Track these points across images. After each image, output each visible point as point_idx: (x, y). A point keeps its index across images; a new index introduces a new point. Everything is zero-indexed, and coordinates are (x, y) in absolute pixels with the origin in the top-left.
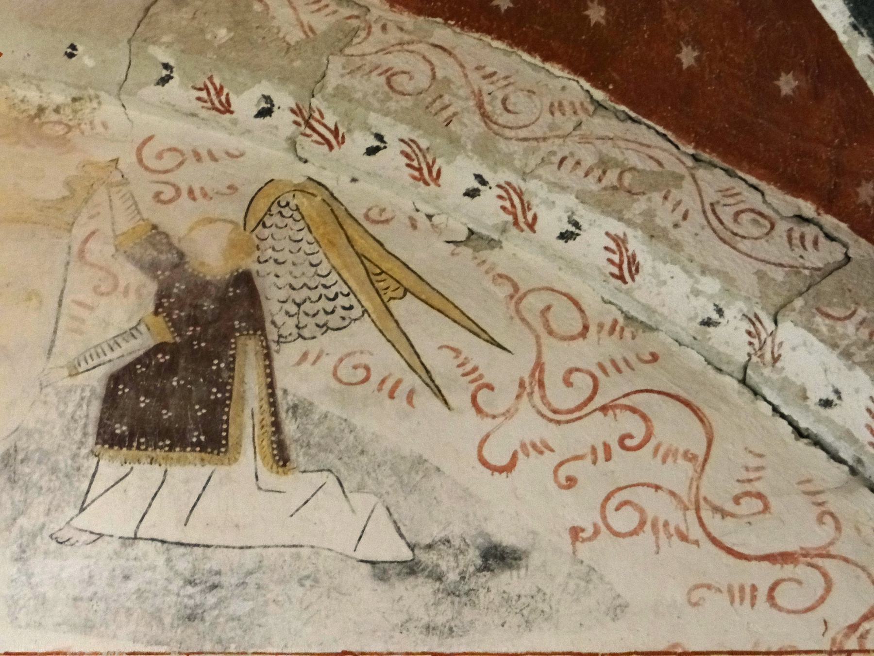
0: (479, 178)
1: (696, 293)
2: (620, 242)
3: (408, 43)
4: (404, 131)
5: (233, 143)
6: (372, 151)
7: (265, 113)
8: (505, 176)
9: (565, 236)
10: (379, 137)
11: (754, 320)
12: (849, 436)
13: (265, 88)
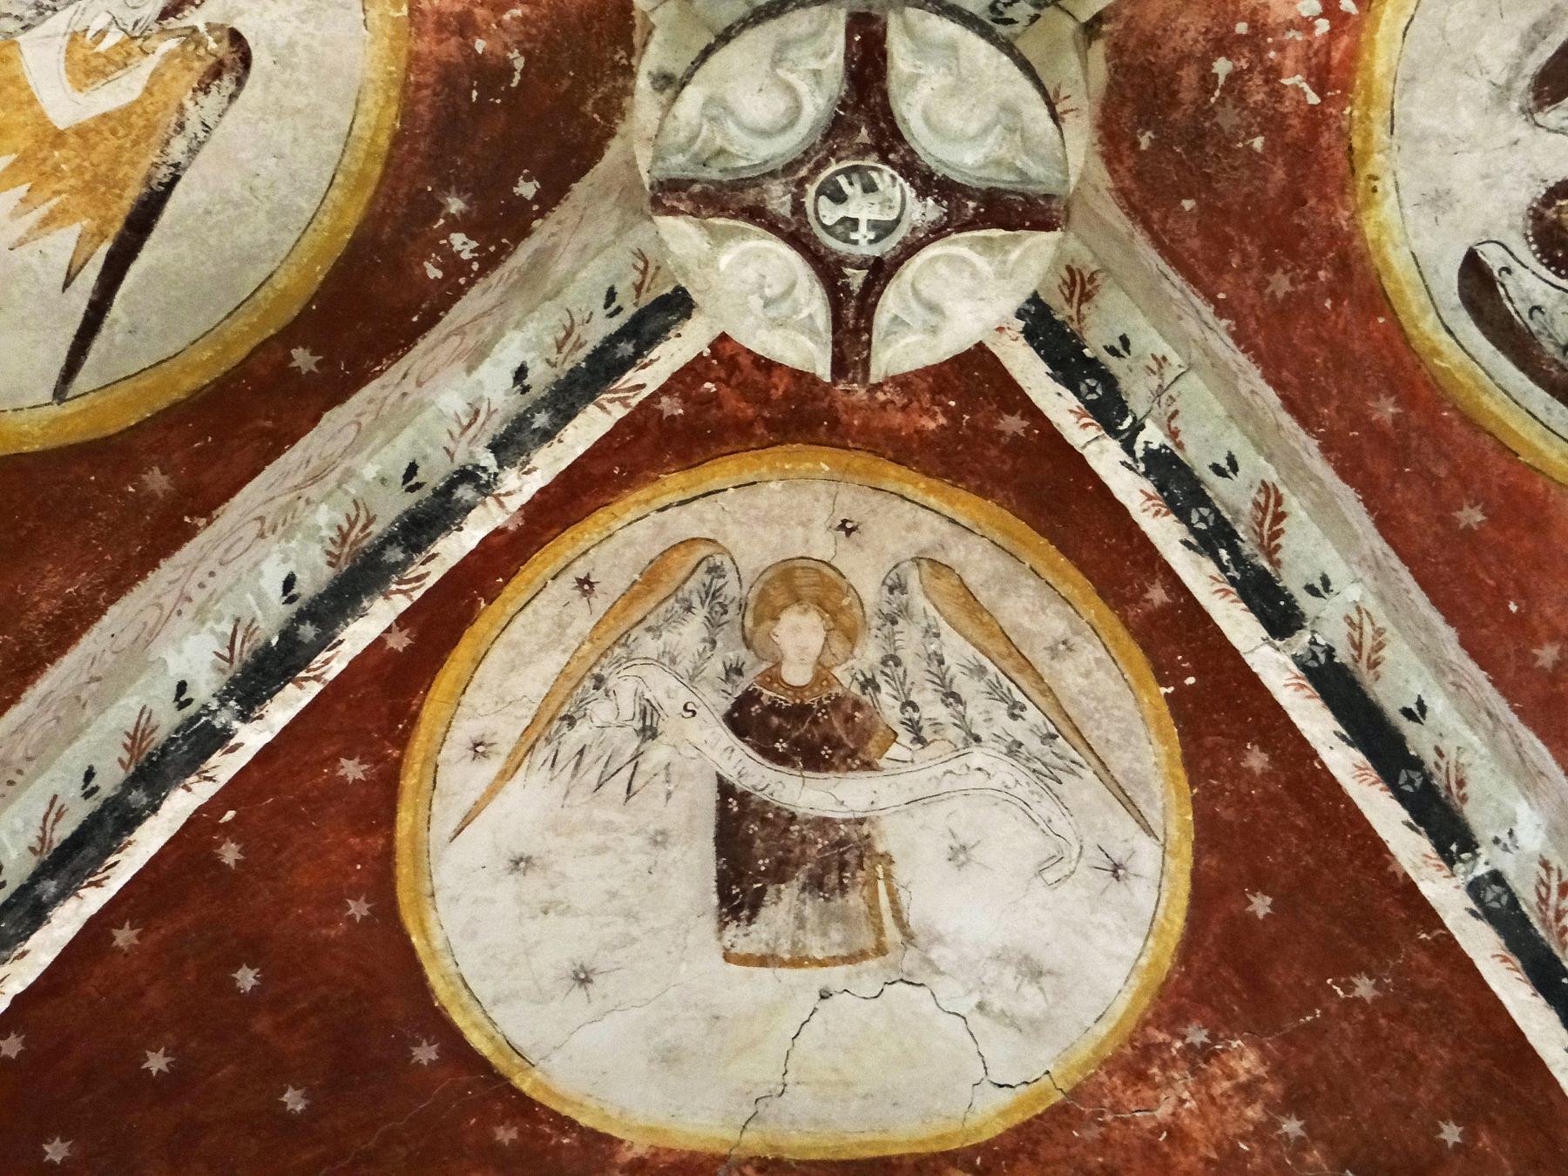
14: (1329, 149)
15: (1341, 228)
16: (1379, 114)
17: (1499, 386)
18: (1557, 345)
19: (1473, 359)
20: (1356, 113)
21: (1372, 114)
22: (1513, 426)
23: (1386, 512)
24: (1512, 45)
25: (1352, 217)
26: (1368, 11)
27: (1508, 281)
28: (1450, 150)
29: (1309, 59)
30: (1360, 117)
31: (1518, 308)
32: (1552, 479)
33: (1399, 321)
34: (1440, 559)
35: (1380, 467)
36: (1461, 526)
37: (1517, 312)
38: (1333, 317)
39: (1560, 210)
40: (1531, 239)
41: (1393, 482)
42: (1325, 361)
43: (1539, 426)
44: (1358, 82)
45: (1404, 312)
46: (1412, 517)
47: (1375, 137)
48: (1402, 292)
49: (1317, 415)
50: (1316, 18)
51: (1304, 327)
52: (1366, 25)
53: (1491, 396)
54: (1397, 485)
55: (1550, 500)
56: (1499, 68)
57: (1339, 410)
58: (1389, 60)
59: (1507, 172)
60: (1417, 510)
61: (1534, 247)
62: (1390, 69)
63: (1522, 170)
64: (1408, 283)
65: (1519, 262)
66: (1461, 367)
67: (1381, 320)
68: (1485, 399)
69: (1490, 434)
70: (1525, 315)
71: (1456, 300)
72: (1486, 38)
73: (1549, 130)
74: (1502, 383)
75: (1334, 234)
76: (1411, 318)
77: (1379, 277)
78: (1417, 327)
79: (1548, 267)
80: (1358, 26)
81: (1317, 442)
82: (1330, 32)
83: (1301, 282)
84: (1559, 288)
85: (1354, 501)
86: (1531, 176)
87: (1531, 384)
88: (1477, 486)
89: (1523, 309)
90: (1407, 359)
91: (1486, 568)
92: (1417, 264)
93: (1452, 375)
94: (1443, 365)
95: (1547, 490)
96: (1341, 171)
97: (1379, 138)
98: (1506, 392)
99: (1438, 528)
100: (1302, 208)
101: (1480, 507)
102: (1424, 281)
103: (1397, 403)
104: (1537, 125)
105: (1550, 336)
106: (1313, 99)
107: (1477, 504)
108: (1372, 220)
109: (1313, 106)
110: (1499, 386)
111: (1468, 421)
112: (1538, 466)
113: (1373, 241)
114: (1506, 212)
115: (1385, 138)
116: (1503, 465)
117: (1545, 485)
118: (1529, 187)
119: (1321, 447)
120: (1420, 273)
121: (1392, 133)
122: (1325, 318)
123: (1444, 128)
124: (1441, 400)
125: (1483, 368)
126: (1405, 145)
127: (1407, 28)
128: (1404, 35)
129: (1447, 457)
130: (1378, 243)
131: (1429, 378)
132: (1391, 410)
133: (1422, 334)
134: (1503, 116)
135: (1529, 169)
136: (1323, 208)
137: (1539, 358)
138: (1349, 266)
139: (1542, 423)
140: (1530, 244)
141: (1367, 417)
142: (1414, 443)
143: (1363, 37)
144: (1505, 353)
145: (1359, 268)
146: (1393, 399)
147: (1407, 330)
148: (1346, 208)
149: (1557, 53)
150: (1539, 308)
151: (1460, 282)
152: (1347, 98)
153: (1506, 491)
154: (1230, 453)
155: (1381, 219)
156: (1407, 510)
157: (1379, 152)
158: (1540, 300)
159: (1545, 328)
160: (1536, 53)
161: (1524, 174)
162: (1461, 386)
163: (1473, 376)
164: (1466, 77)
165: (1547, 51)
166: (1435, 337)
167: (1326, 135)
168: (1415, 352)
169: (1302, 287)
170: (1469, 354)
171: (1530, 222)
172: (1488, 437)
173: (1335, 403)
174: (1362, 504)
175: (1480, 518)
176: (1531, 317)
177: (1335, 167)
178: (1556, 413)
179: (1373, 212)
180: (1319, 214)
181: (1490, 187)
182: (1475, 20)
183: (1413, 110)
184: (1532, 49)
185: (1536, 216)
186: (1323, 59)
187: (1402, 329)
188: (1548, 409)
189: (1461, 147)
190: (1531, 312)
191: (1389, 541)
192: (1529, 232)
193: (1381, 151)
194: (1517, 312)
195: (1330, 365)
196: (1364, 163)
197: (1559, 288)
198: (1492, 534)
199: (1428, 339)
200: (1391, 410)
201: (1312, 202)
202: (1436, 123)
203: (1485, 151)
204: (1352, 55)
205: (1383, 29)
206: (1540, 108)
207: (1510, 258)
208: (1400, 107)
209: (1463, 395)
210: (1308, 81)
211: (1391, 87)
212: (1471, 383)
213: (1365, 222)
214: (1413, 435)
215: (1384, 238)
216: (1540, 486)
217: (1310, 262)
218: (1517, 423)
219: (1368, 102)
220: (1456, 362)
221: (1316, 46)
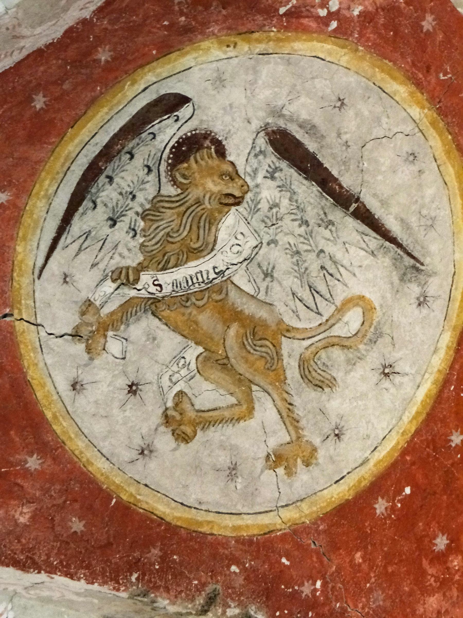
14: (253, 20)
15: (208, 28)
16: (270, 47)
17: (112, 117)
18: (133, 148)
19: (129, 103)
20: (272, 34)
21: (271, 43)
22: (89, 125)
23: (45, 55)
24: (304, 115)
25: (214, 34)
26: (330, 36)
27: (171, 121)
28: (248, 86)
29: (305, 7)
30: (269, 36)
31: (155, 126)
32: (56, 147)
33: (153, 62)
34: (16, 84)
35: (71, 52)
36: (34, 96)
37: (153, 126)
38: (158, 26)
39: (209, 148)
40: (194, 132)
41: (62, 59)
42: (135, 21)
43: (87, 139)
44: (290, 34)
45: (158, 64)
46: (42, 69)
47: (259, 45)
48: (169, 63)
49: (104, 18)
50: (328, 8)
51: (154, 10)
52: (321, 36)
53: (107, 113)
54: (60, 61)
55: (45, 146)
56: (292, 110)
57: (106, 29)
58: (300, 50)
59: (232, 118)
60: (45, 71)
61: (189, 134)
62: (296, 51)
63: (234, 127)
64: (174, 67)
65: (182, 126)
66: (125, 96)
67: (154, 52)
68: (105, 110)
69: (85, 113)
70: (150, 131)
71: (163, 92)
72: (309, 101)
73: (254, 140)
74: (113, 119)
75: (205, 24)
76: (154, 69)
77: (179, 50)
78: (149, 71)
79: (177, 142)
80: (321, 32)
81: (88, 17)
82: (319, 17)
83: (179, 7)
84: (165, 148)
85: (54, 36)
86: (230, 131)
87: (112, 134)
88: (57, 106)
89: (154, 130)
90: (131, 66)
91: (10, 109)
92: (184, 70)
93: (120, 92)
94: (126, 87)
95: (50, 144)
96: (240, 28)
97: (257, 47)
98: (109, 120)
99: (34, 83)
100: (221, 6)
101: (44, 107)
102: (175, 74)
103: (107, 61)
104: (258, 133)
105: (138, 144)
106: (282, 10)
107: (46, 105)
108: (211, 45)
109: (278, 10)
110: (112, 117)
111: (93, 101)
112: (65, 139)
113: (200, 46)
114: (210, 119)
115: (257, 51)
116: (67, 120)
117: (54, 142)
118: (223, 130)
119: (85, 19)
120: (180, 72)
121: (260, 54)
122: (158, 21)
123: (260, 82)
124: (106, 86)
125: (123, 108)
126: (252, 62)
127: (318, 58)
128: (313, 57)
129: (74, 89)
130: (199, 49)
131: (120, 79)
132: (103, 58)
133: (145, 74)
134: (264, 114)
135: (233, 130)
136: (220, 18)
137: (126, 139)
138: (186, 33)
139: (89, 141)
140: (191, 132)
141: (100, 45)
142: (83, 71)
143: (315, 35)
144: (130, 121)
145: (185, 39)
146: (109, 59)
147: (148, 66)
148: (219, 31)
149: (297, 140)
150: (154, 138)
151: (172, 94)
152: (281, 29)
153: (51, 122)
154: (171, 451)
155: (212, 50)
156: (46, 67)
157: (249, 47)
158: (158, 138)
159: (143, 141)
160: (298, 129)
161: (231, 127)
162: (114, 96)
163: (119, 103)
164: (288, 92)
165: (299, 135)
166: (143, 81)
167: (262, 19)
168: (135, 71)
169: (177, 8)
170: (131, 100)
171: (203, 132)
172: (83, 111)
173: (110, 27)
174: (51, 41)
175: (38, 107)
176: (149, 134)
177: (243, 24)
178: (94, 149)
179: (216, 46)
180: (217, 15)
181: (224, 109)
182: (320, 94)
183: (271, 65)
184: (301, 126)
185: (207, 135)
186: (305, 14)
187: (148, 63)
188: (97, 144)
189: (248, 92)
190: (152, 133)
191: (28, 56)
192: (198, 132)
193: (250, 49)
194: (153, 126)
195: (131, 24)
196: (243, 40)
197: (165, 148)
198: (28, 114)
199: (142, 78)
200: (103, 58)
201: (224, 12)
202: (263, 77)
203: (245, 106)
204: (306, 30)
205: (318, 45)
206: (267, 134)
207: (184, 121)
208: (274, 58)
209: (108, 98)
210: (293, 6)
211: (286, 52)
212: (115, 101)
213: (211, 41)
214: (88, 71)
215: (201, 52)
216: (54, 140)
217: (190, 12)
218: (91, 126)
219: (278, 40)
220: (127, 94)
221: (312, 10)
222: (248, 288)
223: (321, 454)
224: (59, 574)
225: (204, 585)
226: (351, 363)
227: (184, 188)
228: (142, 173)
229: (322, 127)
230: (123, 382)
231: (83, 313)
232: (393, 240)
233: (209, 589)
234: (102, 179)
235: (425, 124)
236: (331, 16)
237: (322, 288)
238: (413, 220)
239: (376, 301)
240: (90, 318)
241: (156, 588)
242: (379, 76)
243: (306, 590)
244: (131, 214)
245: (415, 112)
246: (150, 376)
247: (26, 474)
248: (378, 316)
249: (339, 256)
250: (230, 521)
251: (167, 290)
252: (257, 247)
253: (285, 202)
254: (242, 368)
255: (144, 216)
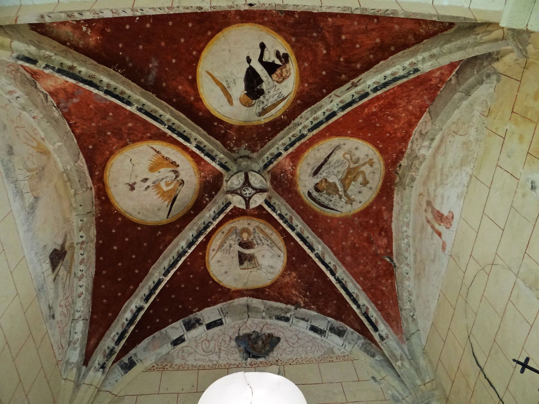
0: (83, 270)
1: (80, 307)
2: (82, 294)
3: (43, 92)
4: (86, 258)
5: (76, 234)
6: (81, 254)
7: (81, 237)
8: (85, 274)
9: (80, 286)
10: (83, 254)
11: (80, 317)
12: (73, 338)
13: (85, 236)
16: (298, 178)
24: (310, 170)
31: (314, 196)
165: (314, 170)
185: (315, 187)
204: (295, 172)
222: (341, 175)
223: (371, 158)
224: (84, 328)
225: (393, 175)
226: (355, 155)
227: (324, 189)
228: (322, 197)
229: (313, 166)
230: (359, 195)
231: (347, 203)
232: (333, 151)
233: (394, 173)
234: (324, 204)
235: (313, 149)
236: (292, 168)
237: (341, 163)
238: (330, 148)
239: (344, 153)
240: (348, 202)
241: (394, 183)
242: (303, 158)
243: (395, 157)
244: (330, 198)
245: (310, 151)
246: (357, 190)
247: (376, 208)
248: (346, 152)
249: (335, 160)
250: (382, 172)
251: (342, 189)
252: (334, 175)
253: (326, 171)
254: (355, 174)
255: (329, 196)
